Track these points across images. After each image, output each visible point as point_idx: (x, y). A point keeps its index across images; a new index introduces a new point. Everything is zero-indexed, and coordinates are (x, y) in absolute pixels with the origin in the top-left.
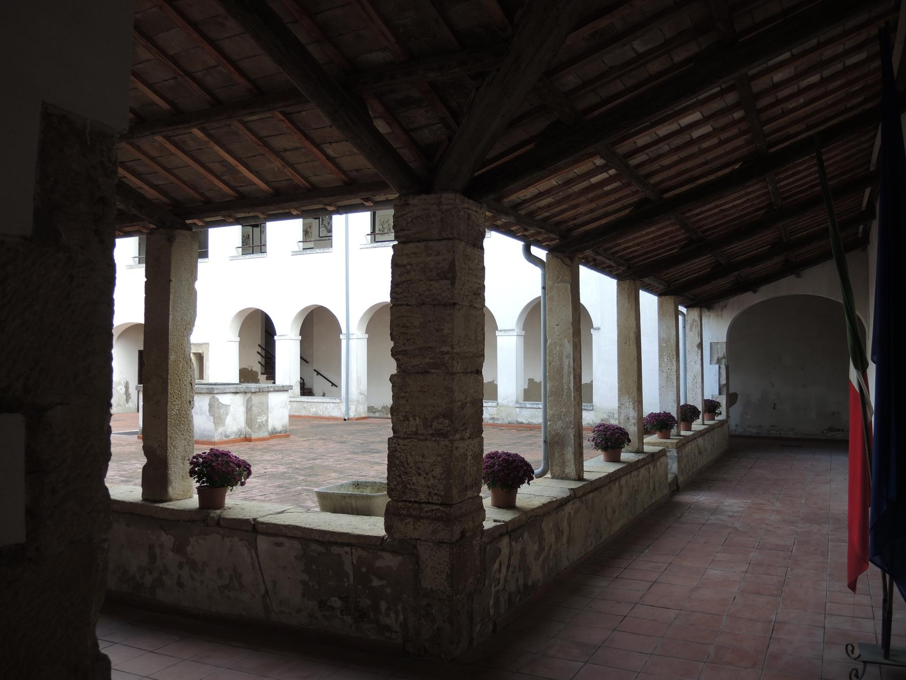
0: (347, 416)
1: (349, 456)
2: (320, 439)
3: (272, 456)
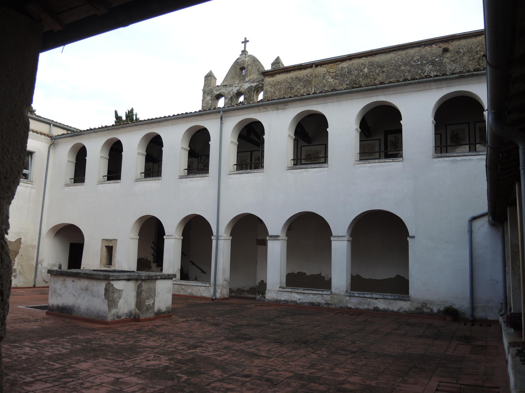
0: (214, 297)
1: (226, 343)
2: (197, 320)
3: (155, 341)
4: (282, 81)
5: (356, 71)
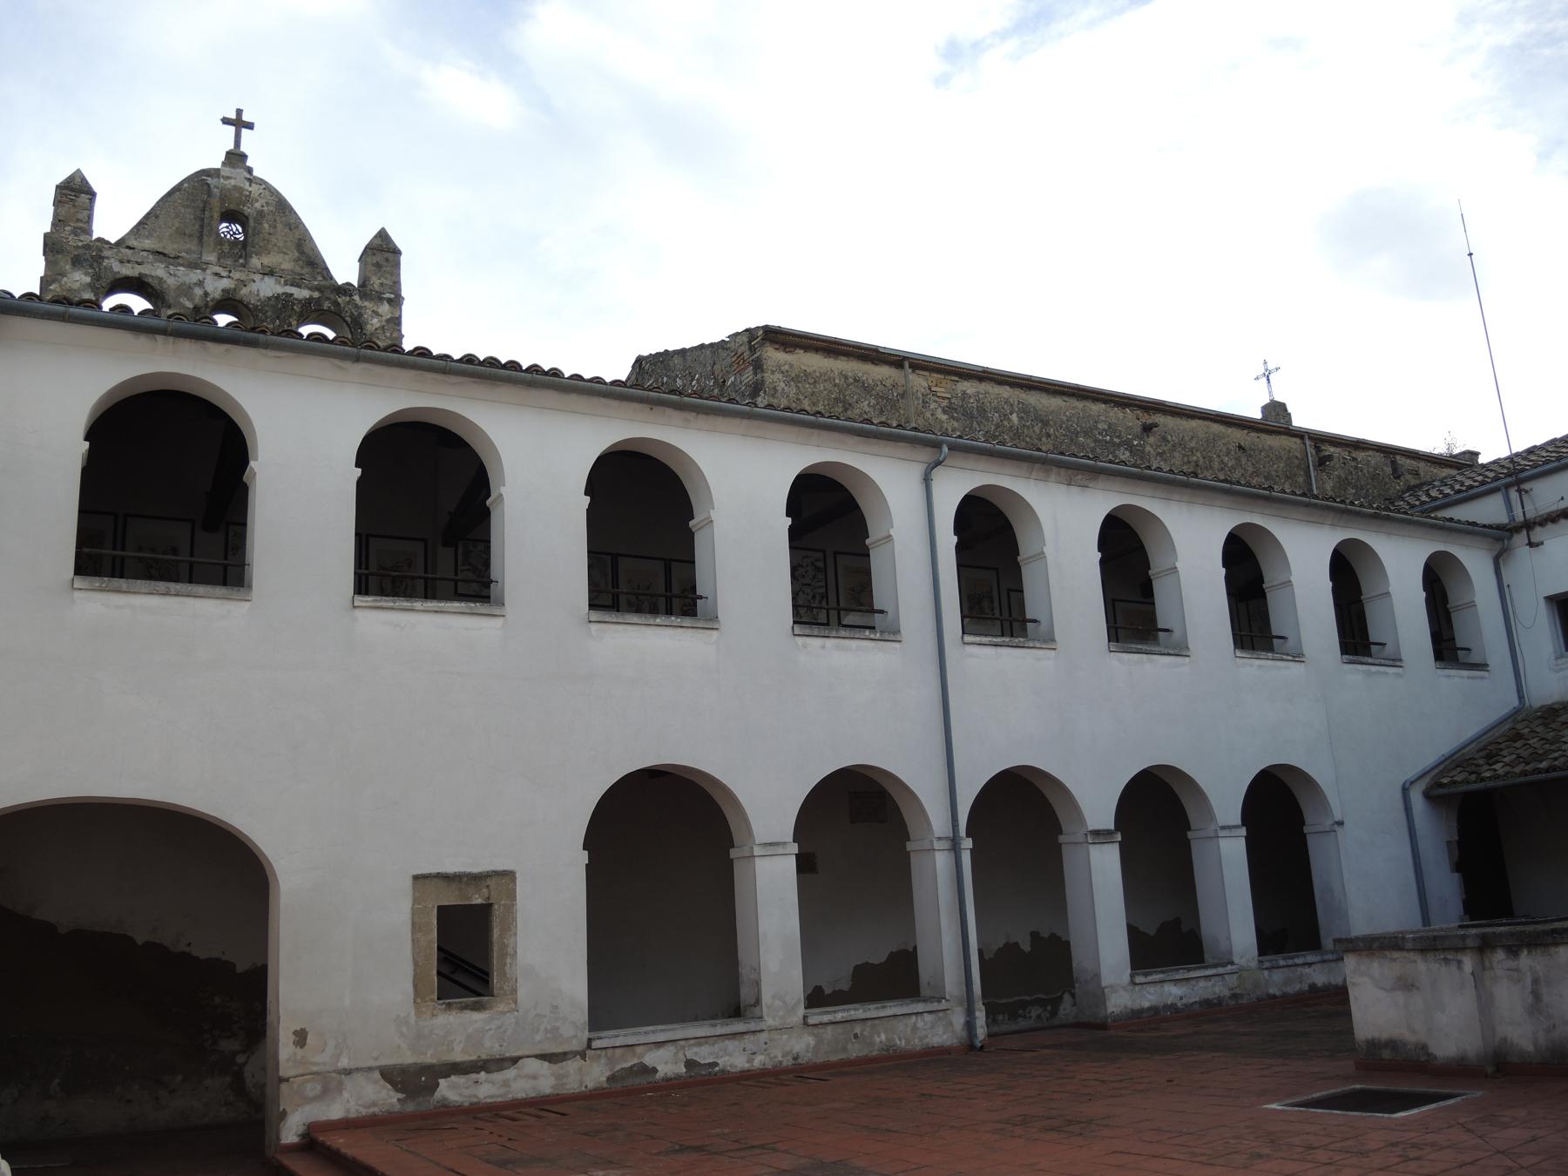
4: (818, 374)
5: (996, 414)
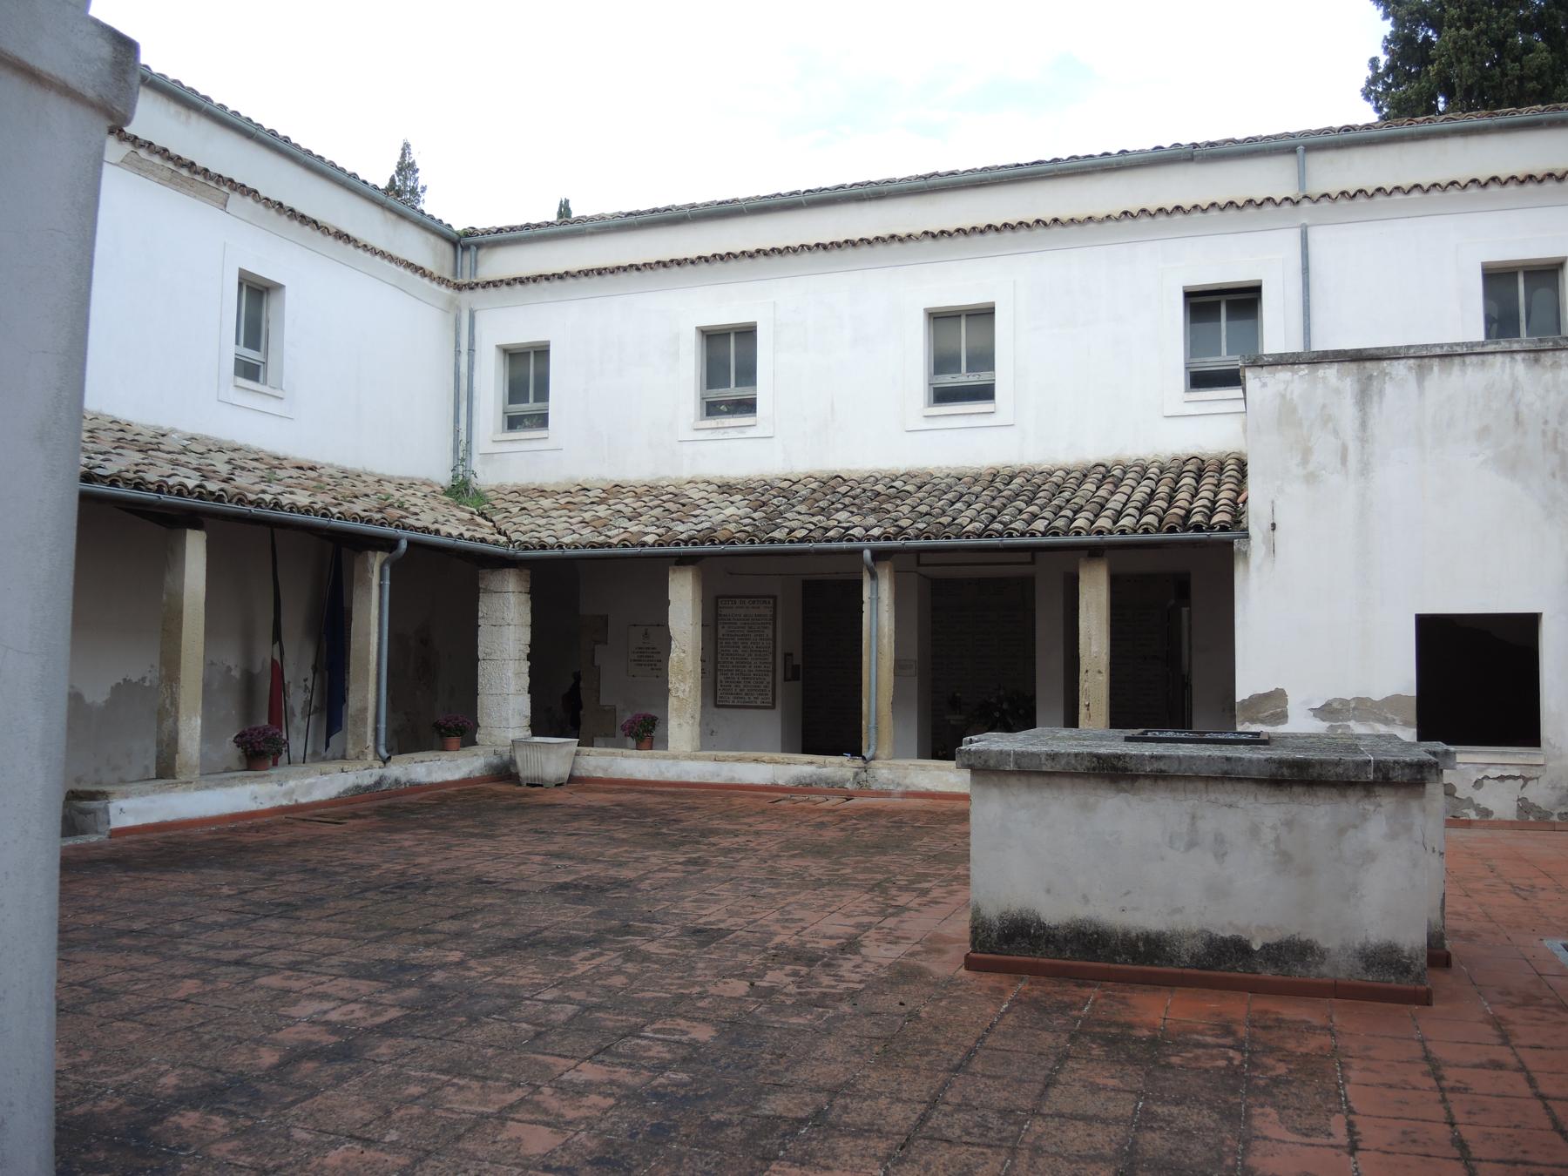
1: (626, 873)
